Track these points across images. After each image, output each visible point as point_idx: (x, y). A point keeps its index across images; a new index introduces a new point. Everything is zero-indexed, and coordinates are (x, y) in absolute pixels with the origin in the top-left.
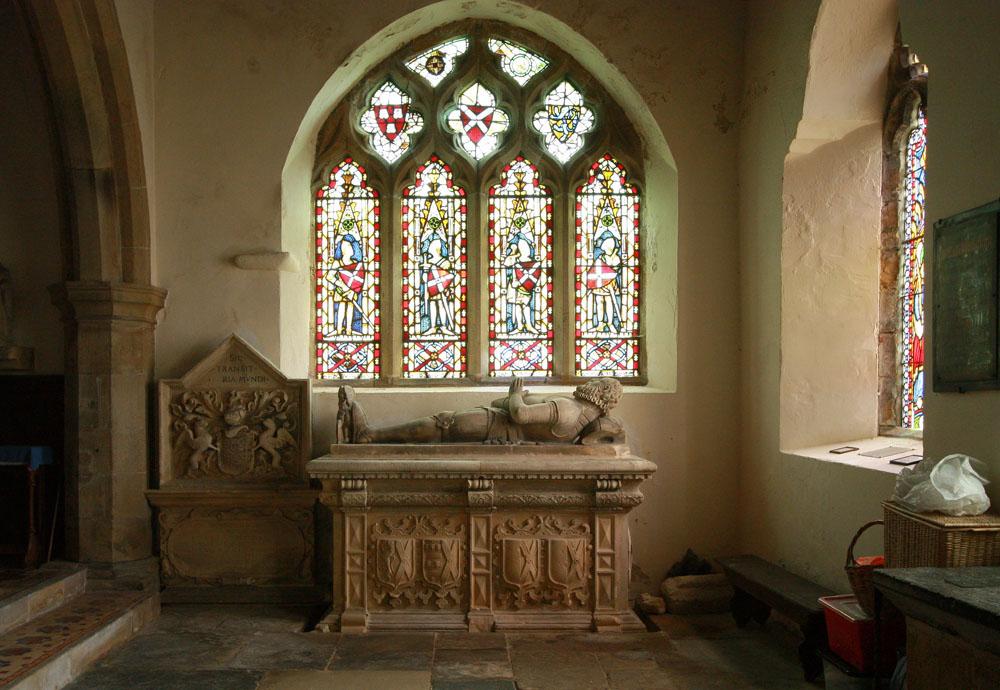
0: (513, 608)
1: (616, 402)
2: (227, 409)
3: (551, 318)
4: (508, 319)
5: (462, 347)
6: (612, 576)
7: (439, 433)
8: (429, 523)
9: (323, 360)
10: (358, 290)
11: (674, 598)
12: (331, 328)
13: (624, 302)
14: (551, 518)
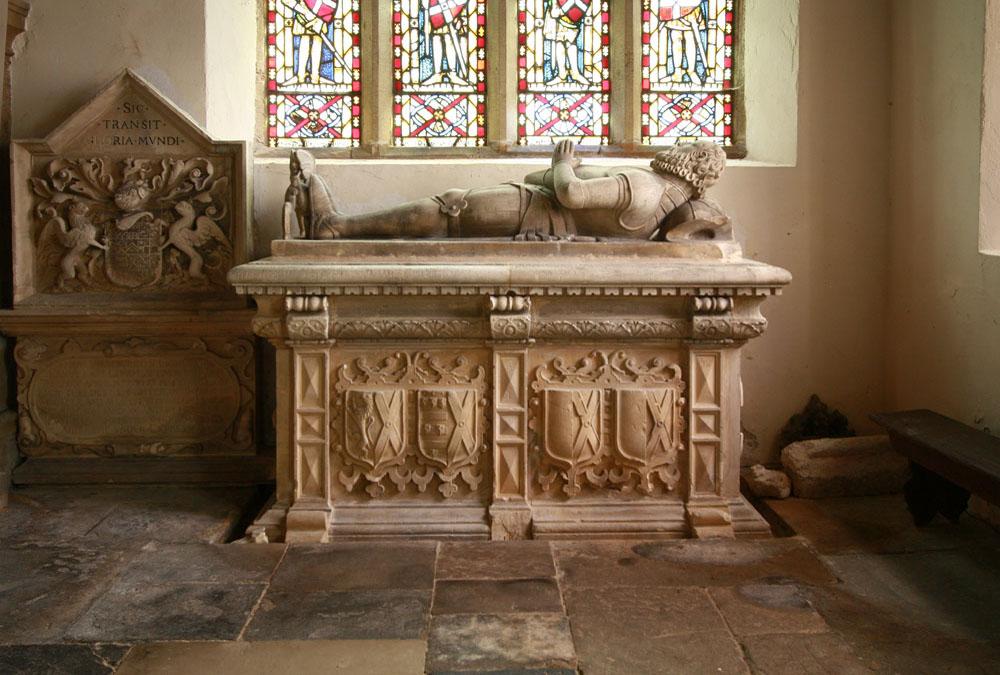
0: (561, 496)
1: (716, 177)
2: (120, 186)
3: (607, 62)
4: (545, 62)
5: (479, 103)
6: (716, 446)
7: (444, 223)
8: (428, 364)
9: (277, 120)
10: (328, 18)
11: (804, 474)
12: (290, 73)
13: (712, 39)
14: (620, 357)
